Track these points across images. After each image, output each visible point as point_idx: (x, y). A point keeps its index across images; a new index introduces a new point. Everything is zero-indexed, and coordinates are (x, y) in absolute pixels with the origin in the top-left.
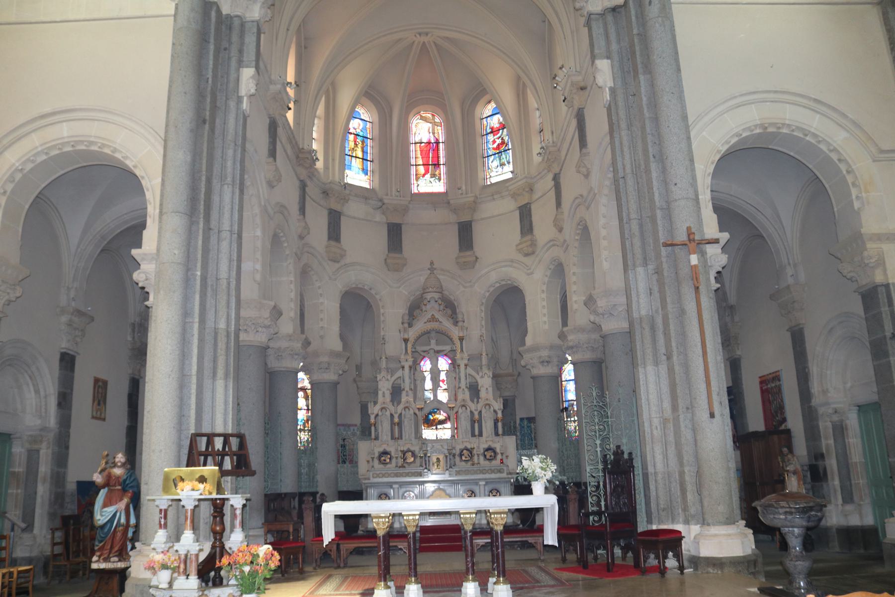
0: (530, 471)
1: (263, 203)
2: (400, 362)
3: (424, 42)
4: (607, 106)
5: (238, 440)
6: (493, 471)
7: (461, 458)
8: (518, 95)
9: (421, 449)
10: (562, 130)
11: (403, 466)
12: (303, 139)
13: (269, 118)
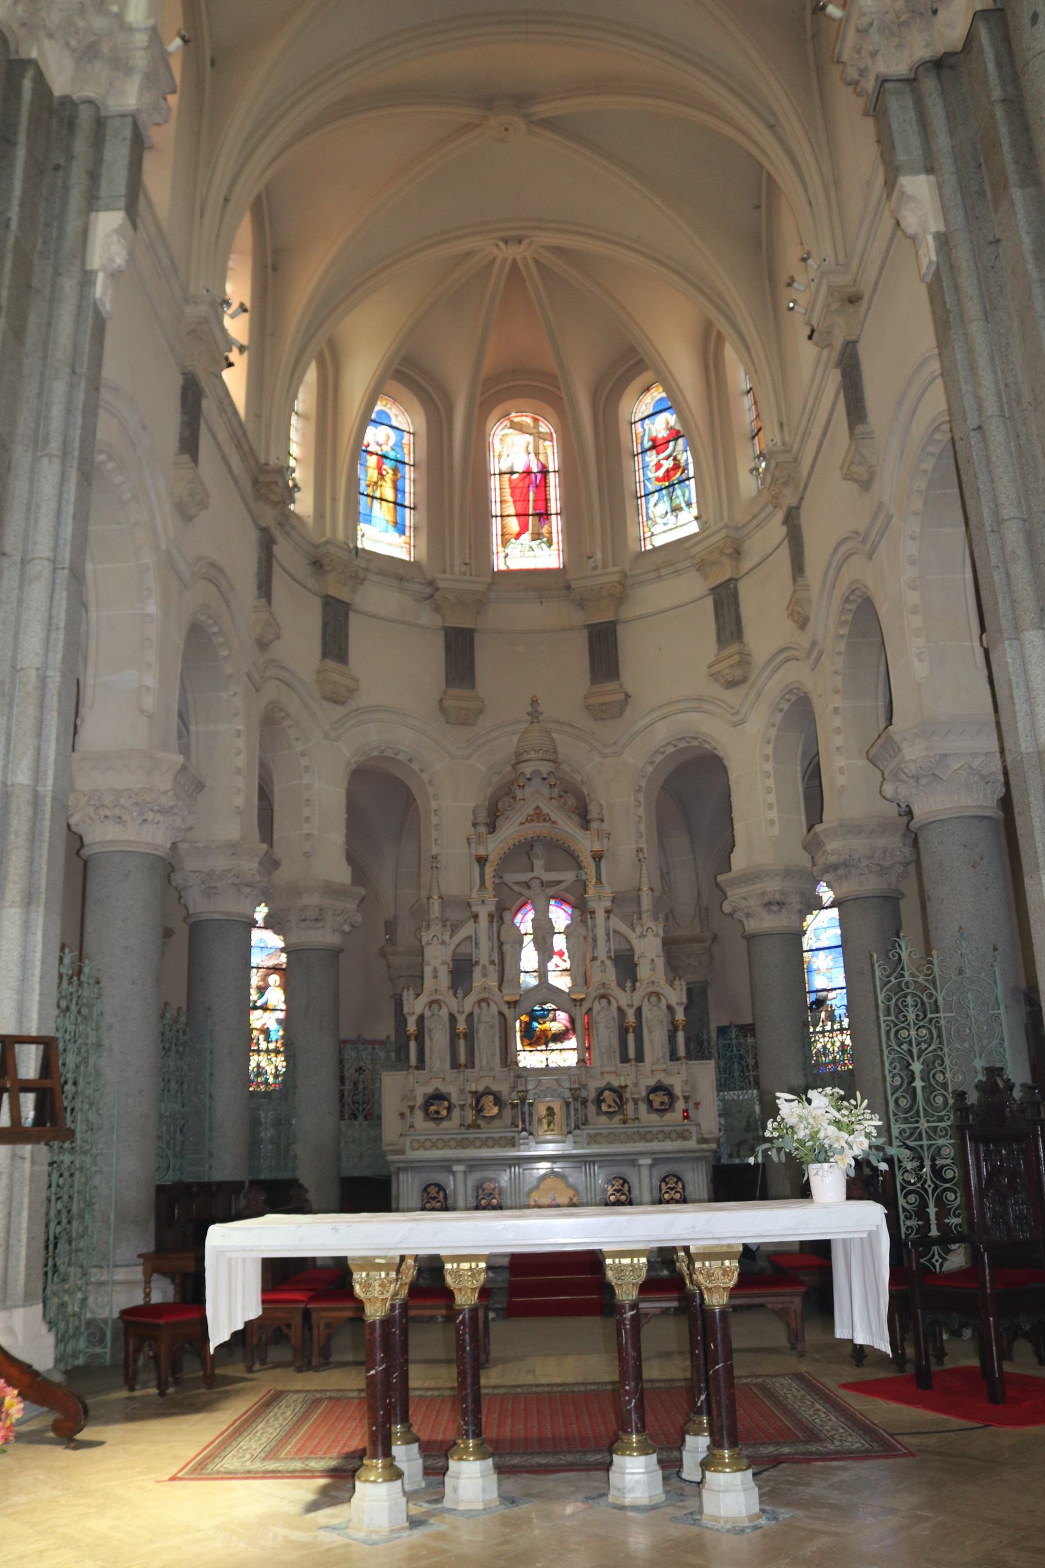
0: (801, 1134)
1: (163, 546)
2: (469, 905)
3: (514, 260)
4: (928, 279)
5: (41, 1047)
6: (667, 1136)
7: (599, 1107)
8: (706, 368)
9: (513, 1088)
10: (803, 413)
11: (475, 1126)
12: (268, 448)
13: (183, 374)
